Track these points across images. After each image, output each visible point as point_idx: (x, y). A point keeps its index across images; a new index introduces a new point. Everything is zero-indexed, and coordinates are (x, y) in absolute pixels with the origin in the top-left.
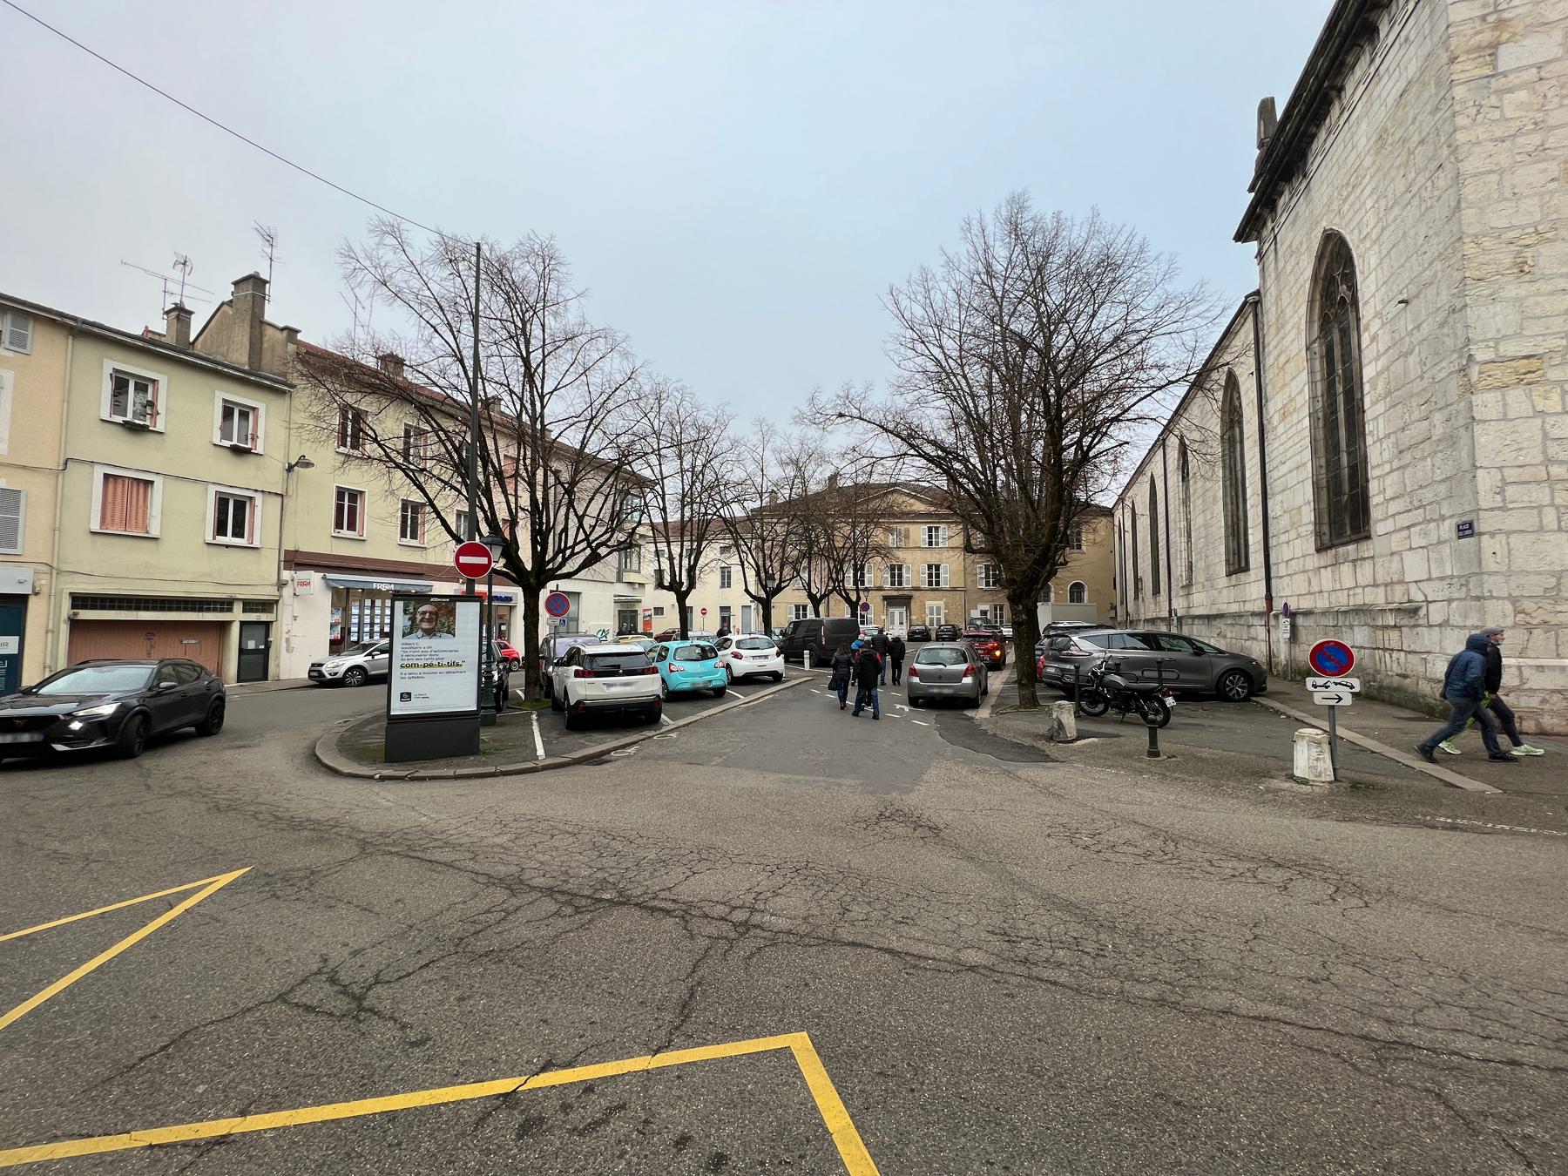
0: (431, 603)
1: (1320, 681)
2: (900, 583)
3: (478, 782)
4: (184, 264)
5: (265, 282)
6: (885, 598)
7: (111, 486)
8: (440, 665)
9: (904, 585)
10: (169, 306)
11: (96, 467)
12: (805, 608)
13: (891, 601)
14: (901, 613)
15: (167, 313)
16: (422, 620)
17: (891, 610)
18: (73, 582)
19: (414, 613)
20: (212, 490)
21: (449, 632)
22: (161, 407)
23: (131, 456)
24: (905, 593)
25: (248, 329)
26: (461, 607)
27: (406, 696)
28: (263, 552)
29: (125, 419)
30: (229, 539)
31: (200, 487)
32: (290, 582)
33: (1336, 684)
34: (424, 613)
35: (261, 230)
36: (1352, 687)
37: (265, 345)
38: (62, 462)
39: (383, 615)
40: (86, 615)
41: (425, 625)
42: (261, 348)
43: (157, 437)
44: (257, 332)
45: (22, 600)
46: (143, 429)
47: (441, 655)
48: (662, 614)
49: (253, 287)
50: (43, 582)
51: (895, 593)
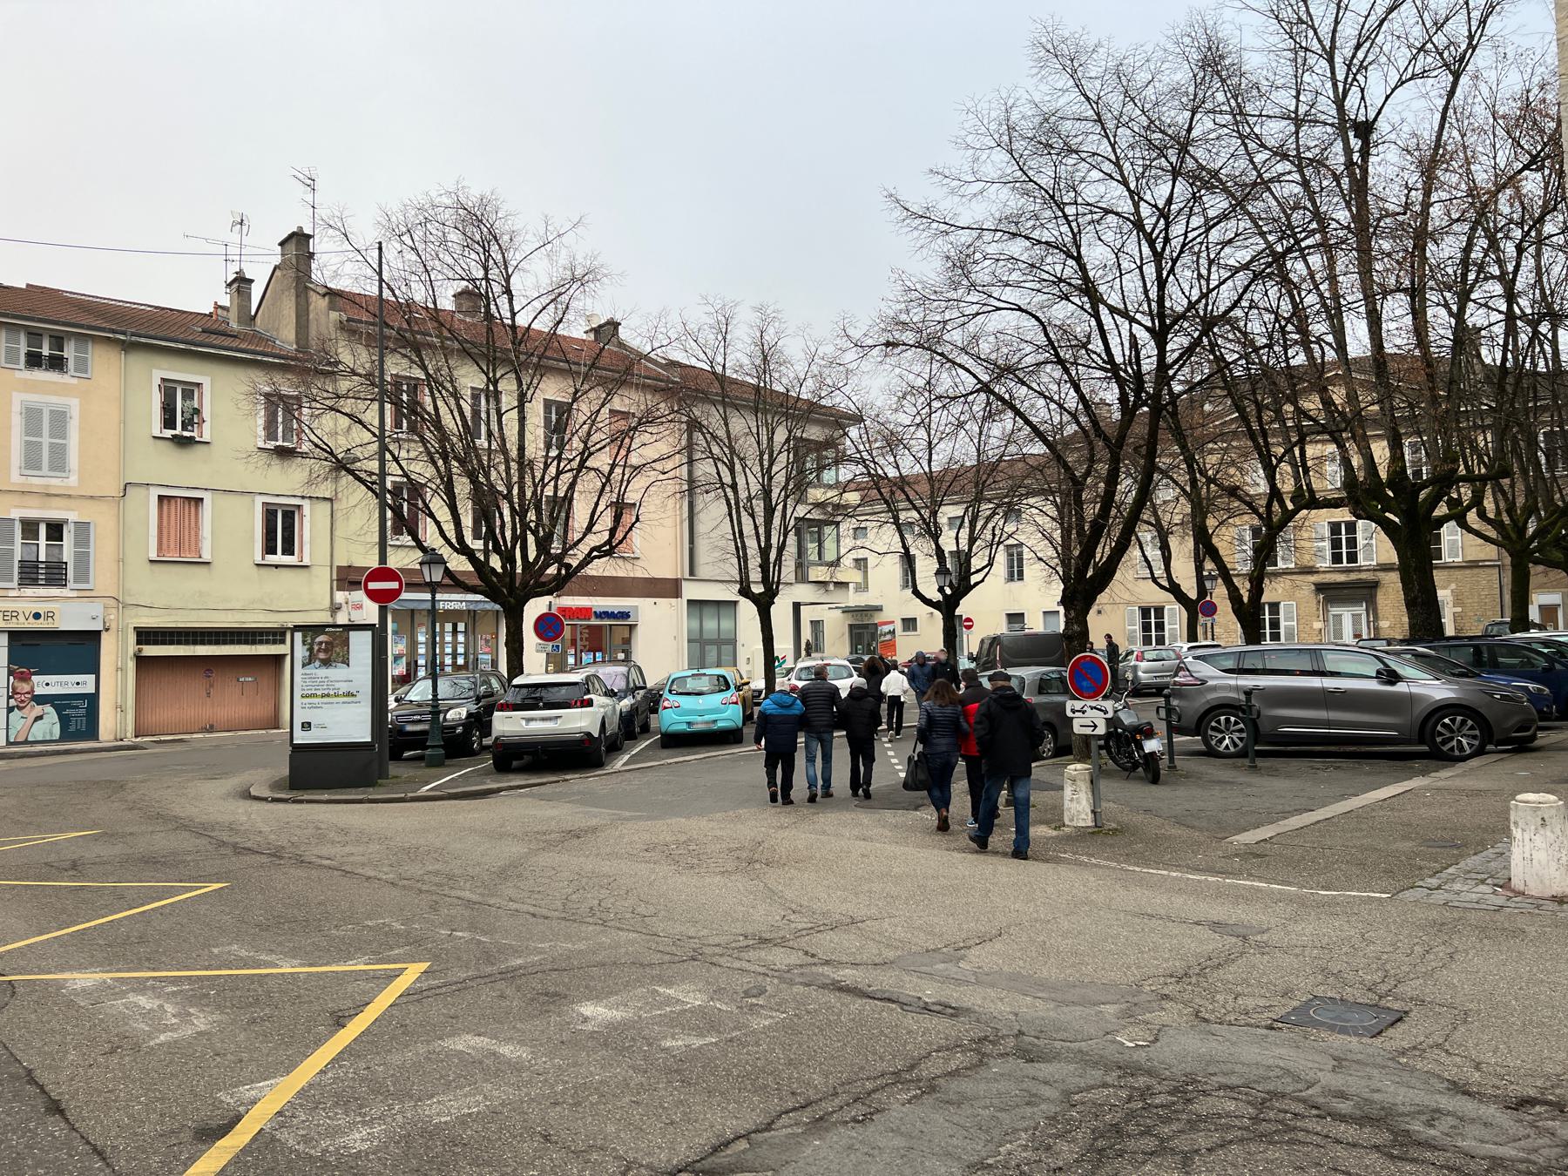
0: (326, 633)
1: (1078, 705)
2: (1352, 558)
3: (344, 806)
4: (241, 223)
5: (309, 237)
6: (1320, 588)
7: (165, 507)
8: (336, 695)
9: (1361, 561)
10: (231, 277)
11: (151, 488)
12: (1160, 611)
13: (1331, 593)
14: (1356, 618)
15: (229, 285)
16: (319, 651)
17: (1335, 610)
18: (137, 616)
19: (311, 645)
20: (260, 500)
21: (343, 662)
22: (206, 414)
23: (181, 472)
24: (1363, 576)
25: (293, 299)
26: (354, 636)
27: (306, 726)
28: (314, 570)
29: (173, 432)
30: (279, 558)
31: (247, 498)
32: (344, 605)
33: (1092, 708)
34: (321, 643)
35: (301, 177)
36: (1106, 712)
37: (311, 316)
38: (122, 487)
39: (443, 643)
40: (151, 651)
41: (322, 656)
42: (308, 320)
43: (205, 446)
44: (303, 302)
45: (95, 635)
46: (190, 442)
47: (337, 685)
48: (915, 629)
49: (298, 242)
50: (112, 617)
51: (1341, 578)
